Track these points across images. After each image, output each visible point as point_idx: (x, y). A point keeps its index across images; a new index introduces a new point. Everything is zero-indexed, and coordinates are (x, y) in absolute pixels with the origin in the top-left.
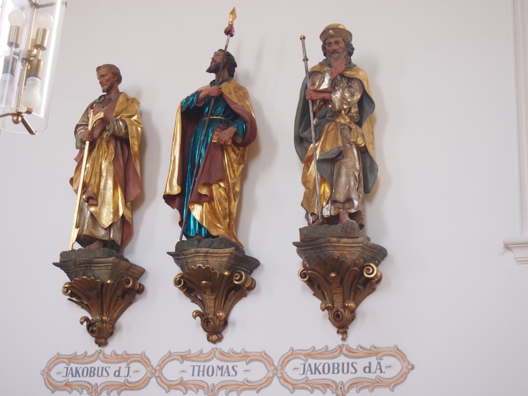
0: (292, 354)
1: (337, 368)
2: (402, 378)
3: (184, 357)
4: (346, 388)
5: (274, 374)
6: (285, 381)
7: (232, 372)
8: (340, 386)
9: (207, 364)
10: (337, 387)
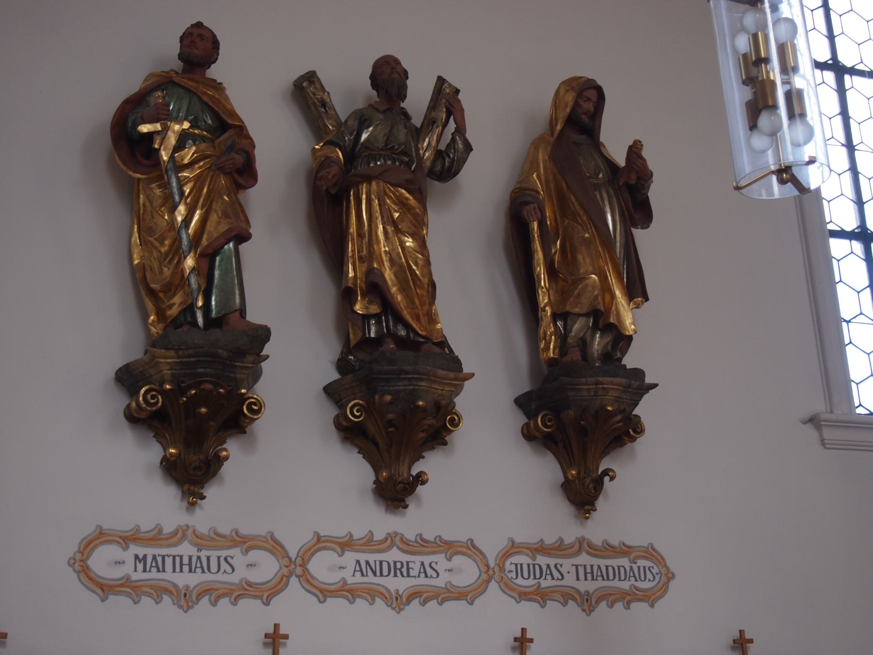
0: (514, 548)
3: (346, 545)
7: (556, 574)
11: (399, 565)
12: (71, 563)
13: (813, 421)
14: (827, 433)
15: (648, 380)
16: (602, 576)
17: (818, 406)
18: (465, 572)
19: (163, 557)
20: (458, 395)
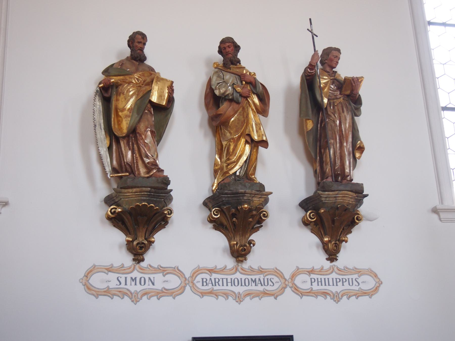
1: (206, 282)
2: (376, 289)
3: (110, 269)
4: (139, 296)
5: (186, 284)
6: (296, 290)
8: (238, 295)
9: (233, 277)
10: (334, 295)
11: (217, 280)
12: (81, 281)
13: (435, 211)
14: (443, 215)
15: (365, 193)
16: (261, 283)
17: (436, 203)
18: (174, 282)
19: (223, 279)
20: (361, 205)
